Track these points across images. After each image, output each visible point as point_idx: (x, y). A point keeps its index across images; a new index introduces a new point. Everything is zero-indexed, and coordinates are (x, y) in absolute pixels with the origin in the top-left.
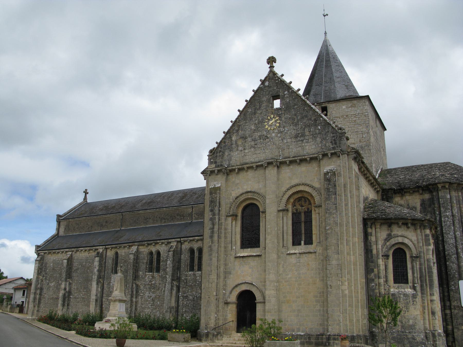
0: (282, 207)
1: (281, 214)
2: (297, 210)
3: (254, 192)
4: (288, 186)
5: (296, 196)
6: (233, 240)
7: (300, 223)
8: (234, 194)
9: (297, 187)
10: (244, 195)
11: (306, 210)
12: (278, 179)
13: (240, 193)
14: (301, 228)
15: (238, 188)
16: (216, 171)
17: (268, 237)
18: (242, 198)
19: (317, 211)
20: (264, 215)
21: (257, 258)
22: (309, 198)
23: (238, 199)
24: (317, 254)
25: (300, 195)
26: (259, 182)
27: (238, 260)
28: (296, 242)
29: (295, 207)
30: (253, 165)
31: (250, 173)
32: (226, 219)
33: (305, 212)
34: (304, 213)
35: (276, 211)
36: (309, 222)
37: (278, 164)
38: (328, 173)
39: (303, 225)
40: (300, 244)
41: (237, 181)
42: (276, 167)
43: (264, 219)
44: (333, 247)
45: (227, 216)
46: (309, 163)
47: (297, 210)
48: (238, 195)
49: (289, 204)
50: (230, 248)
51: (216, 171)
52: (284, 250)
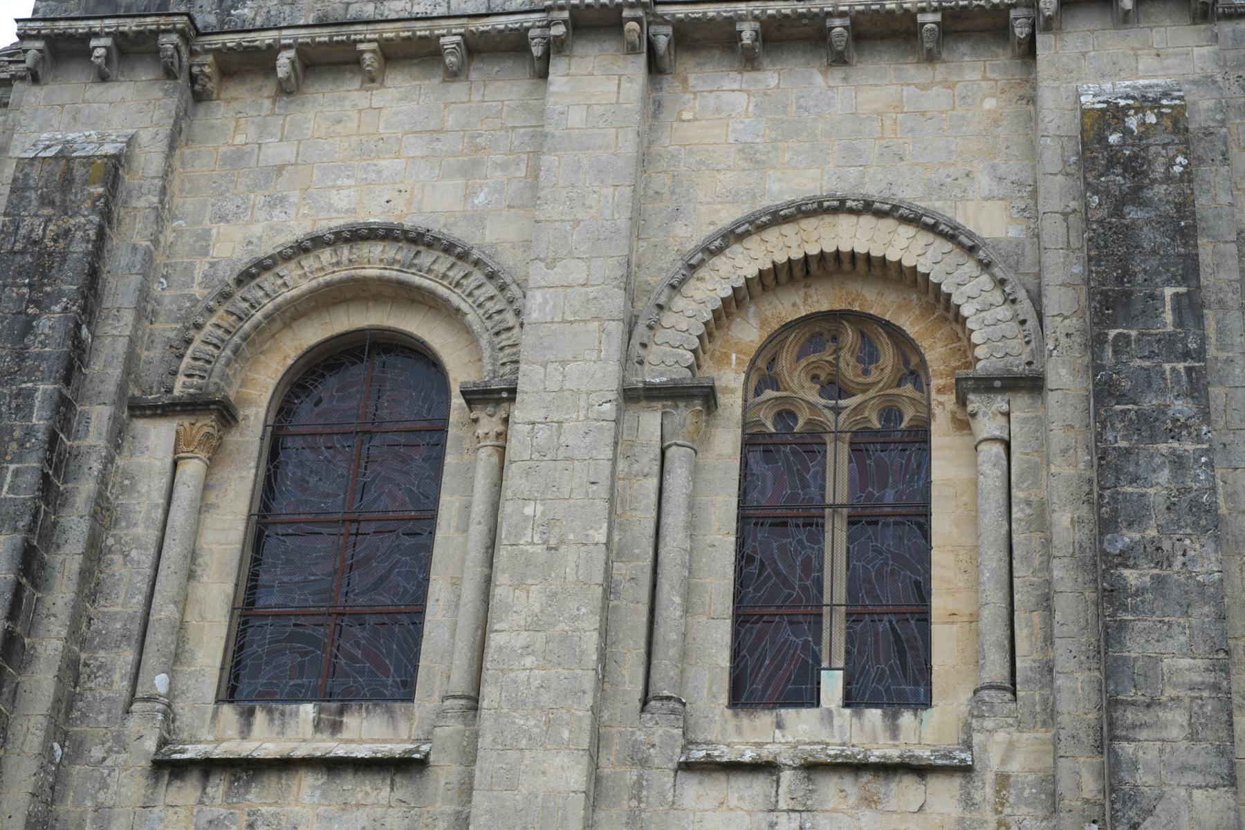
0: (666, 361)
1: (650, 421)
2: (785, 416)
3: (418, 239)
4: (728, 216)
5: (791, 305)
6: (164, 611)
7: (813, 524)
8: (232, 246)
9: (808, 224)
10: (326, 255)
11: (876, 424)
12: (645, 160)
13: (286, 239)
14: (813, 568)
15: (275, 202)
16: (100, 46)
17: (518, 602)
18: (299, 279)
19: (988, 426)
20: (488, 424)
21: (375, 793)
22: (910, 325)
23: (267, 281)
24: (985, 791)
25: (822, 299)
26: (470, 169)
27: (185, 793)
28: (767, 673)
29: (769, 394)
30: (440, 28)
31: (401, 100)
32: (118, 437)
33: (862, 444)
34: (858, 450)
35: (611, 385)
36: (896, 523)
37: (662, 42)
38: (1112, 115)
39: (836, 539)
40: (809, 697)
41: (276, 151)
42: (642, 59)
43: (486, 458)
44: (1178, 717)
45: (139, 409)
46: (931, 58)
47: (785, 416)
48: (266, 249)
49: (723, 360)
50: (121, 685)
51: (100, 46)
52: (659, 733)
